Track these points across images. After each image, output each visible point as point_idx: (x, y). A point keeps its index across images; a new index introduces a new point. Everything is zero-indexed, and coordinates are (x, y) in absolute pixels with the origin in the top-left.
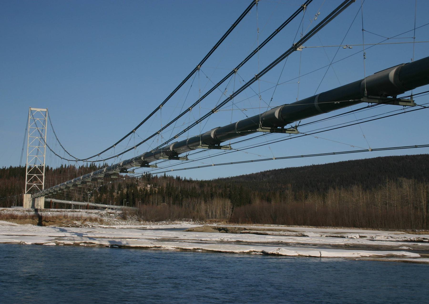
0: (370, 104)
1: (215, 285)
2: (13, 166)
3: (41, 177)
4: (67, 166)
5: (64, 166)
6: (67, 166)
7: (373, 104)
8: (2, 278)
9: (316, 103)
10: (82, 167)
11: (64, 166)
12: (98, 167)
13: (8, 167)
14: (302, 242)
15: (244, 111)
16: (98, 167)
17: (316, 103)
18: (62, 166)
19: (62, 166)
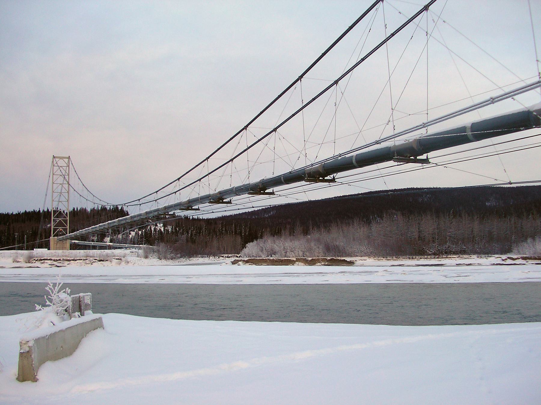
0: (399, 163)
1: (130, 251)
2: (28, 211)
3: (66, 221)
4: (79, 209)
5: (76, 209)
6: (79, 209)
7: (401, 163)
8: (539, 262)
9: (354, 161)
10: (94, 209)
11: (76, 209)
12: (108, 209)
13: (23, 211)
14: (399, 141)
15: (436, 21)
16: (108, 209)
17: (354, 161)
18: (74, 209)
19: (74, 209)
